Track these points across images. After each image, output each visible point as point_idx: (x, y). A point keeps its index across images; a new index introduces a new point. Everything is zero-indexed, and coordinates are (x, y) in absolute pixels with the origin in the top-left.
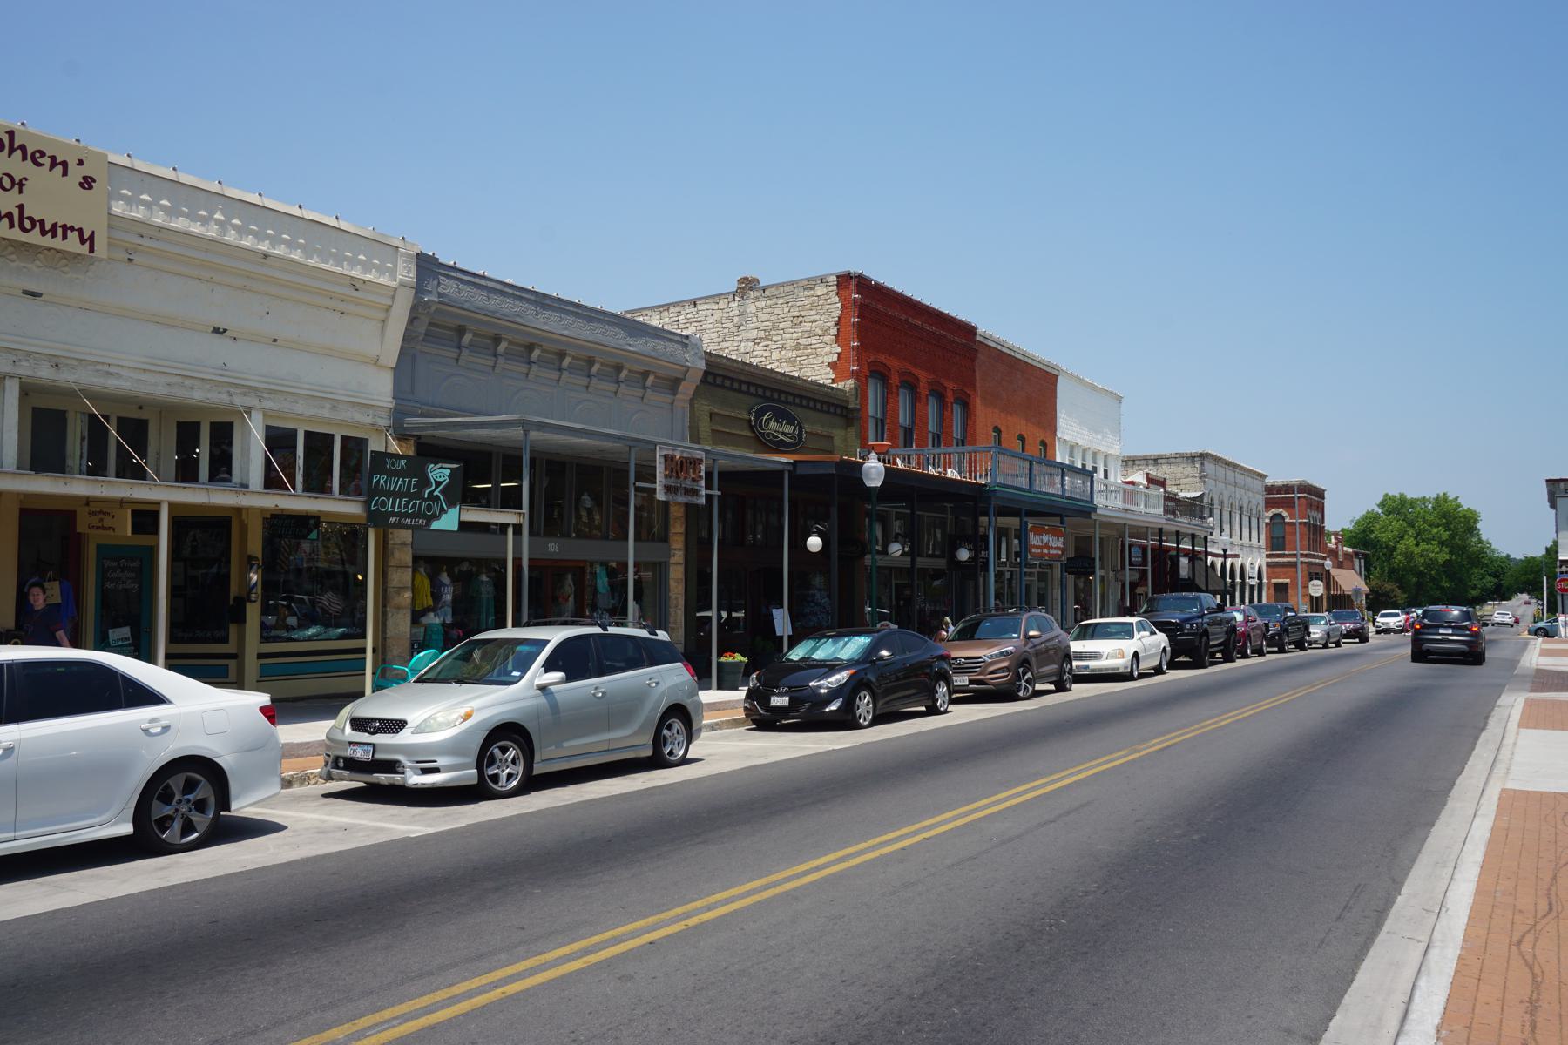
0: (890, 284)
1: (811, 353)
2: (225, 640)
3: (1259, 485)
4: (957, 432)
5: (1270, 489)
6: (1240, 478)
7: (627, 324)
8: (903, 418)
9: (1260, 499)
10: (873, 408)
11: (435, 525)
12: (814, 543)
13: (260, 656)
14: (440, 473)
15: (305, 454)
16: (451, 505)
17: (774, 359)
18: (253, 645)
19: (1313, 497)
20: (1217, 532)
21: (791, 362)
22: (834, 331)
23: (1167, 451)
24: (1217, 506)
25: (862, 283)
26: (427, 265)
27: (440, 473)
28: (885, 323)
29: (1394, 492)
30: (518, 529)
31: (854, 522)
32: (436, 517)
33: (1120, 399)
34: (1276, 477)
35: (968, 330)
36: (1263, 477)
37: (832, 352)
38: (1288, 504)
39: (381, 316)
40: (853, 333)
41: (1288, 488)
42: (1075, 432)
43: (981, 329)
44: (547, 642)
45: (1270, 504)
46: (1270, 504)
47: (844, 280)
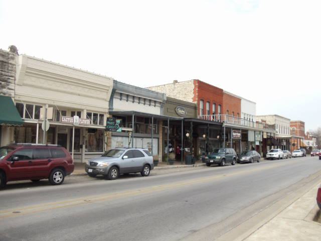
0: (210, 84)
1: (189, 96)
2: (79, 151)
3: (288, 122)
4: (219, 111)
5: (291, 123)
6: (284, 121)
7: (148, 91)
8: (213, 110)
9: (288, 125)
10: (201, 107)
11: (118, 131)
12: (187, 135)
13: (86, 154)
14: (118, 121)
15: (94, 116)
16: (120, 127)
17: (181, 97)
18: (84, 153)
19: (302, 124)
20: (278, 133)
21: (184, 98)
22: (193, 91)
23: (267, 114)
24: (278, 126)
25: (199, 82)
26: (115, 82)
27: (118, 121)
28: (205, 91)
29: (17, 46)
30: (132, 132)
31: (198, 132)
32: (118, 129)
33: (255, 103)
34: (293, 119)
35: (222, 90)
36: (289, 120)
37: (192, 96)
38: (295, 126)
39: (299, 139)
40: (197, 92)
41: (296, 122)
42: (245, 109)
43: (224, 90)
44: (144, 156)
45: (291, 126)
46: (291, 126)
47: (195, 81)
